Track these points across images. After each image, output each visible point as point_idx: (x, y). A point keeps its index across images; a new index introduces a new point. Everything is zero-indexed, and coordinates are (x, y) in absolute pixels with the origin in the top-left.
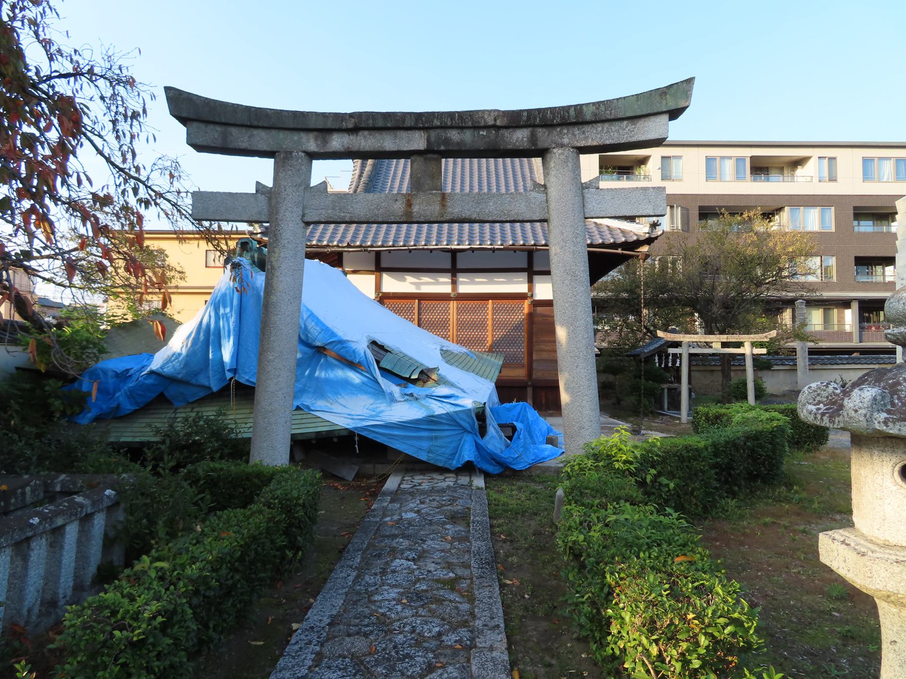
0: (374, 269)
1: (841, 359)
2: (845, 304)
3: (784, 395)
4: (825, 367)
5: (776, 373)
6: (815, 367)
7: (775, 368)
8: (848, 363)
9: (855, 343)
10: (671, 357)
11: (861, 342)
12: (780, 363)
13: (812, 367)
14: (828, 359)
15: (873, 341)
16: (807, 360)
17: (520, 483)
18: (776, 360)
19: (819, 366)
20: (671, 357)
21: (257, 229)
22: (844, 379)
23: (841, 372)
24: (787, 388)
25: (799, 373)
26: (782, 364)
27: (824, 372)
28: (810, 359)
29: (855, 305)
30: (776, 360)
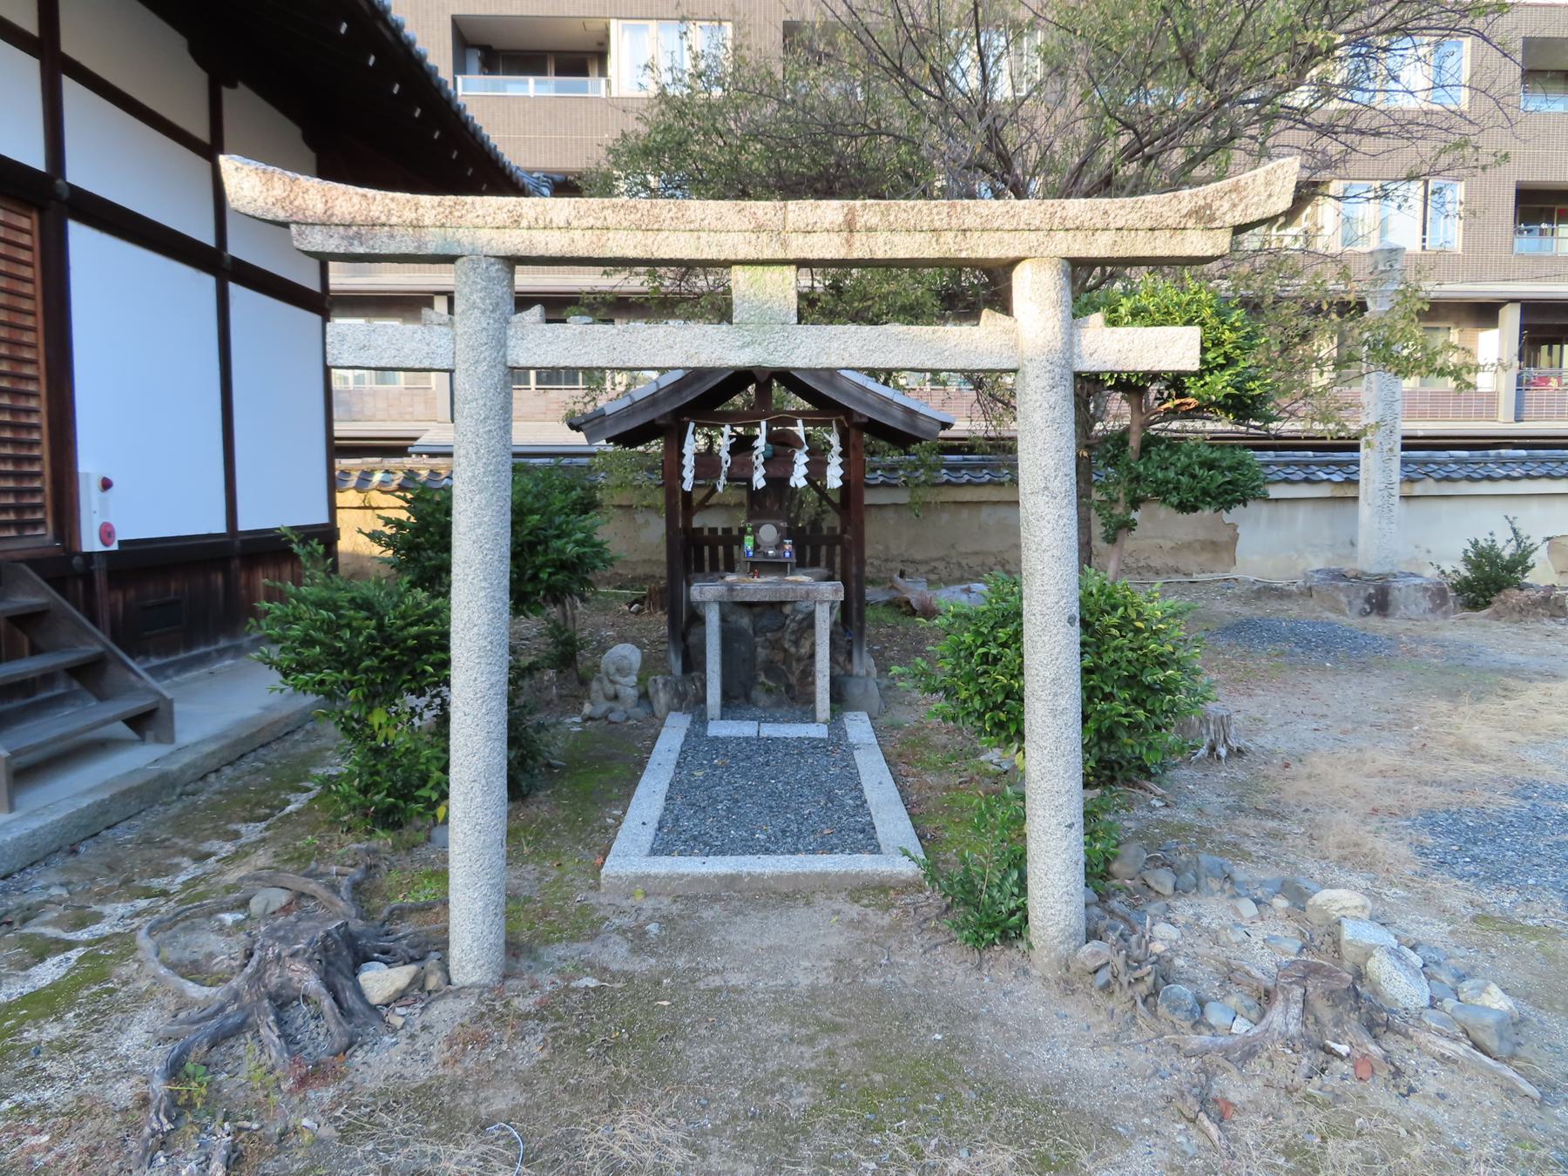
0: (333, 370)
1: (1502, 463)
2: (1484, 312)
3: (1309, 592)
4: (1448, 489)
5: (1284, 509)
6: (1418, 489)
7: (1275, 492)
8: (1528, 477)
9: (1502, 423)
10: (808, 559)
11: (1518, 419)
12: (1301, 475)
13: (1407, 490)
14: (1459, 462)
15: (1549, 418)
16: (1396, 465)
17: (1397, 964)
18: (1287, 464)
19: (1430, 487)
20: (808, 559)
21: (96, 908)
22: (1523, 533)
23: (1513, 509)
24: (1318, 564)
25: (1365, 510)
26: (1307, 481)
27: (1444, 506)
28: (1405, 463)
29: (1511, 318)
30: (1287, 464)
